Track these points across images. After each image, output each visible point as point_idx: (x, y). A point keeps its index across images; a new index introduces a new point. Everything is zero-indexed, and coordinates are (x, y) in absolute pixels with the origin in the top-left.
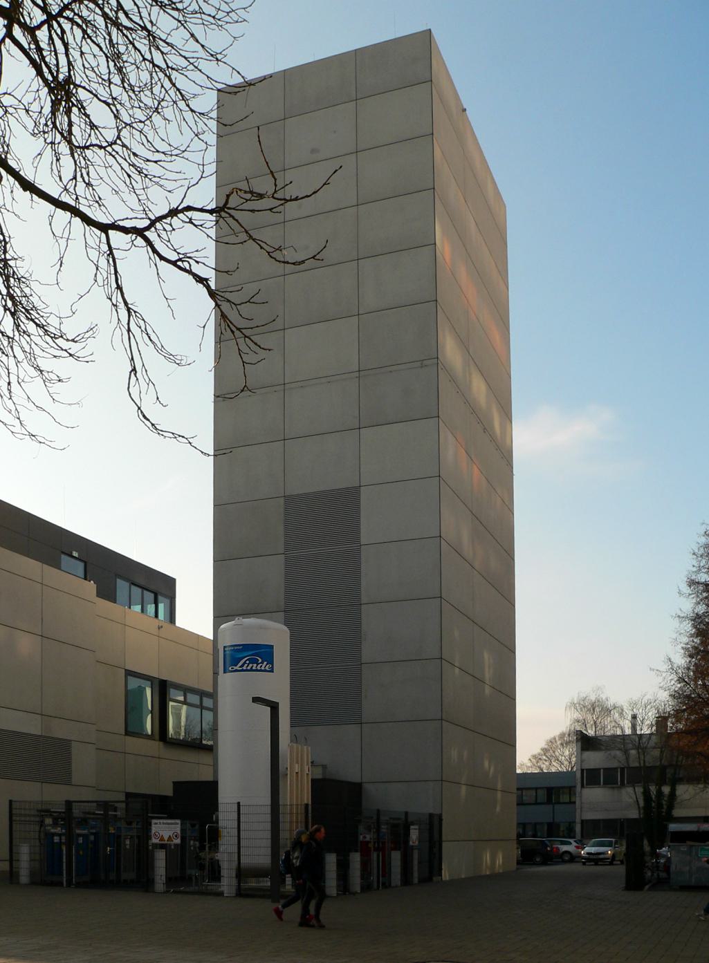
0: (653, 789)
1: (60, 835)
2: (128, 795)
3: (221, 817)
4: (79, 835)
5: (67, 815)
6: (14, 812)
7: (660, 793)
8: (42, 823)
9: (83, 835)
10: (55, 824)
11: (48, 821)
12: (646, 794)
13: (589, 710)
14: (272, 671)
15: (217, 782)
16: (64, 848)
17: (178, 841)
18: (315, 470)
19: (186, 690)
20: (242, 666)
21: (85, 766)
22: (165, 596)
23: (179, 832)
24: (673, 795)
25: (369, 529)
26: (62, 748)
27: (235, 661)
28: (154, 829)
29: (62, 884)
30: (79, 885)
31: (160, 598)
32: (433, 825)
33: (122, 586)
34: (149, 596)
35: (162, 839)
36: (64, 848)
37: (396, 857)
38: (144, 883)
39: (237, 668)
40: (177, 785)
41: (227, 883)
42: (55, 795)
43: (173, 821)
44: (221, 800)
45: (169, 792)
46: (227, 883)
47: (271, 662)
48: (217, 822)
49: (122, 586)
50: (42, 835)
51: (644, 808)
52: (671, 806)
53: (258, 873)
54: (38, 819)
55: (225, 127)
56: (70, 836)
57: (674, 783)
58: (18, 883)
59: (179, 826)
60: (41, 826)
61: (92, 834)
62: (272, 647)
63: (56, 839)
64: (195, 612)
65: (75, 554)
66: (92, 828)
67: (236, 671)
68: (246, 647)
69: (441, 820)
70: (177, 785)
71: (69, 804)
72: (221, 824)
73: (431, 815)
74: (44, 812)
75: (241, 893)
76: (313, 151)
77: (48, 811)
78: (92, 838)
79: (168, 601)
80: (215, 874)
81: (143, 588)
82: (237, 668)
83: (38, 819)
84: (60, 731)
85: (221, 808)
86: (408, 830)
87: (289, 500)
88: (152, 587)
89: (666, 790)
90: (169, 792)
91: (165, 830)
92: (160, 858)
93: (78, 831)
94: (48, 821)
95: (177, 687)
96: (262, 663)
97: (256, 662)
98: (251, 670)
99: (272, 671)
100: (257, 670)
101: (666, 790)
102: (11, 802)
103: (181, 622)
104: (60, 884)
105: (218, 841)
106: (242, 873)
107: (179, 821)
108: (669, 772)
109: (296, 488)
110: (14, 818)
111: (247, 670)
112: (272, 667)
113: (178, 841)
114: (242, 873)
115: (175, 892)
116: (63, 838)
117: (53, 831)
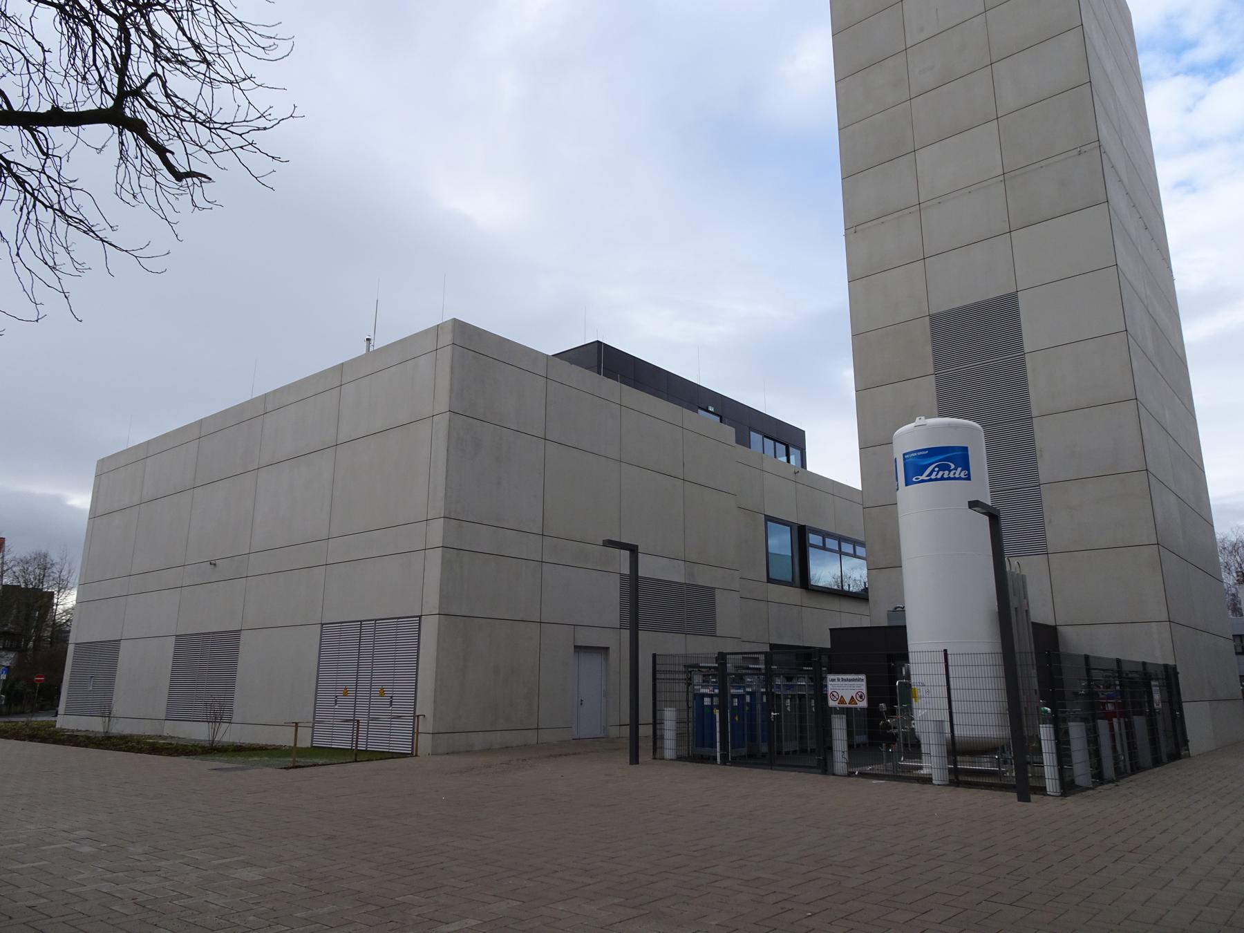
1: (711, 696)
2: (772, 646)
4: (734, 696)
5: (720, 670)
6: (658, 668)
8: (689, 682)
9: (738, 696)
10: (706, 682)
11: (697, 679)
13: (1231, 553)
14: (968, 478)
16: (717, 713)
17: (863, 704)
18: (964, 284)
19: (825, 535)
21: (728, 613)
22: (795, 447)
23: (865, 691)
25: (1032, 334)
26: (705, 596)
27: (921, 470)
30: (738, 761)
31: (791, 449)
32: (1170, 675)
33: (755, 438)
34: (781, 448)
35: (842, 701)
36: (717, 713)
37: (1139, 722)
38: (817, 758)
39: (924, 477)
40: (834, 632)
41: (932, 763)
42: (703, 648)
43: (855, 677)
44: (910, 649)
46: (932, 763)
47: (966, 467)
48: (908, 676)
49: (755, 438)
50: (691, 696)
53: (977, 749)
54: (684, 676)
56: (723, 695)
58: (662, 759)
59: (864, 683)
60: (689, 684)
61: (749, 693)
62: (966, 449)
63: (707, 701)
64: (835, 456)
65: (711, 409)
66: (749, 686)
68: (933, 452)
69: (1176, 674)
70: (834, 632)
71: (722, 657)
72: (914, 680)
73: (1166, 666)
74: (691, 668)
75: (957, 779)
77: (697, 666)
78: (748, 699)
79: (799, 452)
80: (913, 747)
81: (775, 441)
82: (924, 477)
83: (684, 676)
84: (704, 578)
86: (1149, 687)
88: (785, 440)
91: (847, 689)
93: (733, 691)
94: (697, 679)
95: (817, 532)
96: (956, 469)
97: (948, 468)
98: (942, 479)
99: (968, 478)
100: (949, 479)
102: (654, 656)
103: (811, 467)
104: (710, 760)
105: (910, 702)
106: (955, 749)
107: (863, 677)
110: (658, 676)
111: (936, 480)
112: (969, 474)
113: (863, 704)
114: (955, 749)
115: (862, 775)
116: (716, 700)
117: (703, 691)
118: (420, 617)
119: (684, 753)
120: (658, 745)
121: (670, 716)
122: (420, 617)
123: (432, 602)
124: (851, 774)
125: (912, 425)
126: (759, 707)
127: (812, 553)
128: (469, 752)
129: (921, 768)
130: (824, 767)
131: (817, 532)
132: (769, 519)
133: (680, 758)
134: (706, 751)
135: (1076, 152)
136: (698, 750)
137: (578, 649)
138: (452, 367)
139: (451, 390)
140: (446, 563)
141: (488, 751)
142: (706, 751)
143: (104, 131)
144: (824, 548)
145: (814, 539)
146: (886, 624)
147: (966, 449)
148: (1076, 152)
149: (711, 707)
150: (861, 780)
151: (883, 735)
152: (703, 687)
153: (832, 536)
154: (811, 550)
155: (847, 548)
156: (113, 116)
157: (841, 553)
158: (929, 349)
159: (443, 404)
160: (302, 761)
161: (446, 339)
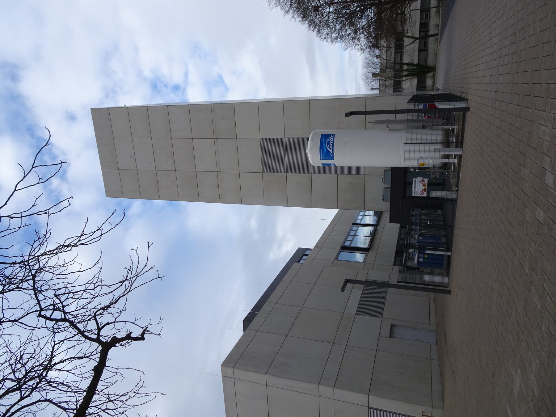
0: (405, 73)
1: (419, 257)
2: (395, 264)
3: (412, 166)
6: (404, 280)
7: (406, 70)
12: (406, 76)
15: (392, 168)
18: (253, 158)
19: (346, 240)
20: (330, 149)
22: (305, 251)
24: (408, 64)
25: (279, 135)
28: (418, 195)
29: (449, 256)
34: (305, 257)
35: (424, 190)
39: (331, 151)
40: (391, 221)
43: (414, 183)
44: (402, 166)
45: (398, 225)
47: (329, 136)
48: (414, 168)
51: (412, 76)
52: (413, 65)
53: (447, 134)
55: (123, 195)
57: (402, 64)
58: (448, 284)
62: (322, 135)
63: (421, 260)
67: (333, 152)
68: (321, 146)
70: (391, 221)
75: (460, 144)
76: (131, 158)
81: (301, 259)
82: (331, 151)
85: (406, 166)
87: (264, 171)
88: (301, 255)
89: (405, 67)
90: (398, 225)
92: (436, 194)
98: (333, 144)
100: (333, 142)
101: (405, 67)
107: (414, 179)
108: (398, 67)
109: (259, 167)
114: (447, 144)
115: (457, 186)
117: (416, 261)
118: (369, 408)
119: (444, 272)
120: (442, 285)
121: (427, 278)
122: (369, 408)
123: (361, 398)
124: (457, 191)
125: (309, 154)
126: (424, 240)
127: (353, 245)
128: (443, 392)
129: (454, 163)
130: (454, 201)
131: (344, 243)
132: (336, 258)
133: (448, 274)
134: (445, 260)
135: (213, 112)
136: (443, 265)
137: (391, 336)
138: (245, 370)
139: (255, 372)
140: (342, 388)
141: (442, 383)
142: (445, 262)
143: (113, 352)
144: (352, 241)
145: (347, 244)
146: (389, 204)
147: (322, 135)
148: (213, 112)
149: (424, 258)
150: (459, 187)
151: (441, 177)
152: (414, 261)
153: (347, 237)
154: (352, 245)
155: (352, 233)
156: (106, 347)
157: (355, 235)
158: (276, 174)
159: (260, 378)
160: (460, 141)
161: (230, 371)
